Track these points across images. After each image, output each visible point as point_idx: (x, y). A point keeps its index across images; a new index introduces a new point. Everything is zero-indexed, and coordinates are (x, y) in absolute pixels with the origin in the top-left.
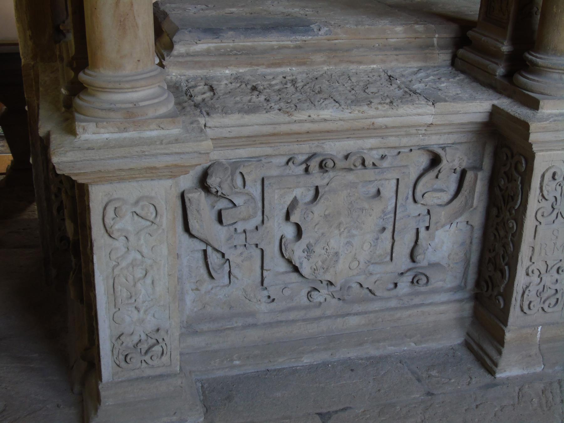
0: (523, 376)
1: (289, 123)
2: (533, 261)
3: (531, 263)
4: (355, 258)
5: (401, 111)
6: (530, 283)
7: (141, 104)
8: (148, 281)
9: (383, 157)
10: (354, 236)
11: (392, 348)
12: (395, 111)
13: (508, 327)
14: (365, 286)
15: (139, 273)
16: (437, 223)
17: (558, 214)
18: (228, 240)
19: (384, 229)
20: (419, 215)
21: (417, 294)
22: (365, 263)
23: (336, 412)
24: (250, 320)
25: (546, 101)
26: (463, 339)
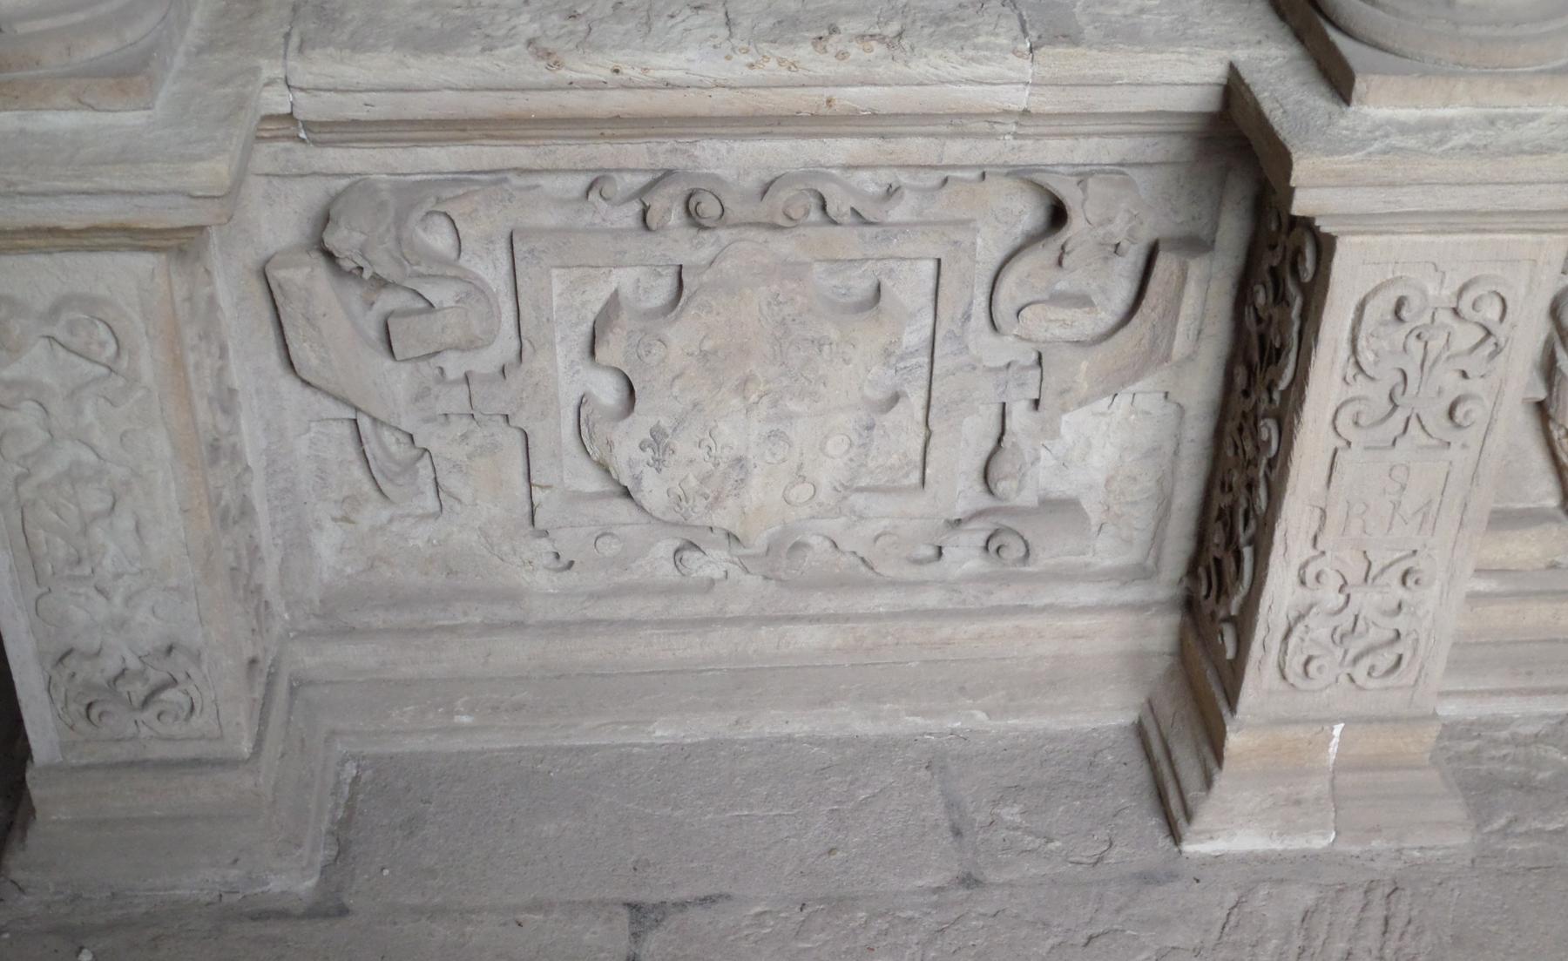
0: (1264, 859)
1: (551, 88)
2: (1320, 546)
3: (1313, 553)
4: (800, 476)
5: (918, 68)
6: (1311, 607)
7: (22, 28)
8: (125, 523)
9: (891, 192)
10: (790, 417)
11: (919, 720)
12: (899, 67)
13: (1238, 716)
14: (845, 545)
15: (95, 501)
16: (1063, 392)
17: (1408, 420)
18: (417, 400)
19: (895, 398)
20: (1009, 365)
21: (1006, 580)
22: (835, 489)
23: (682, 905)
24: (505, 612)
25: (1376, 79)
26: (1127, 718)
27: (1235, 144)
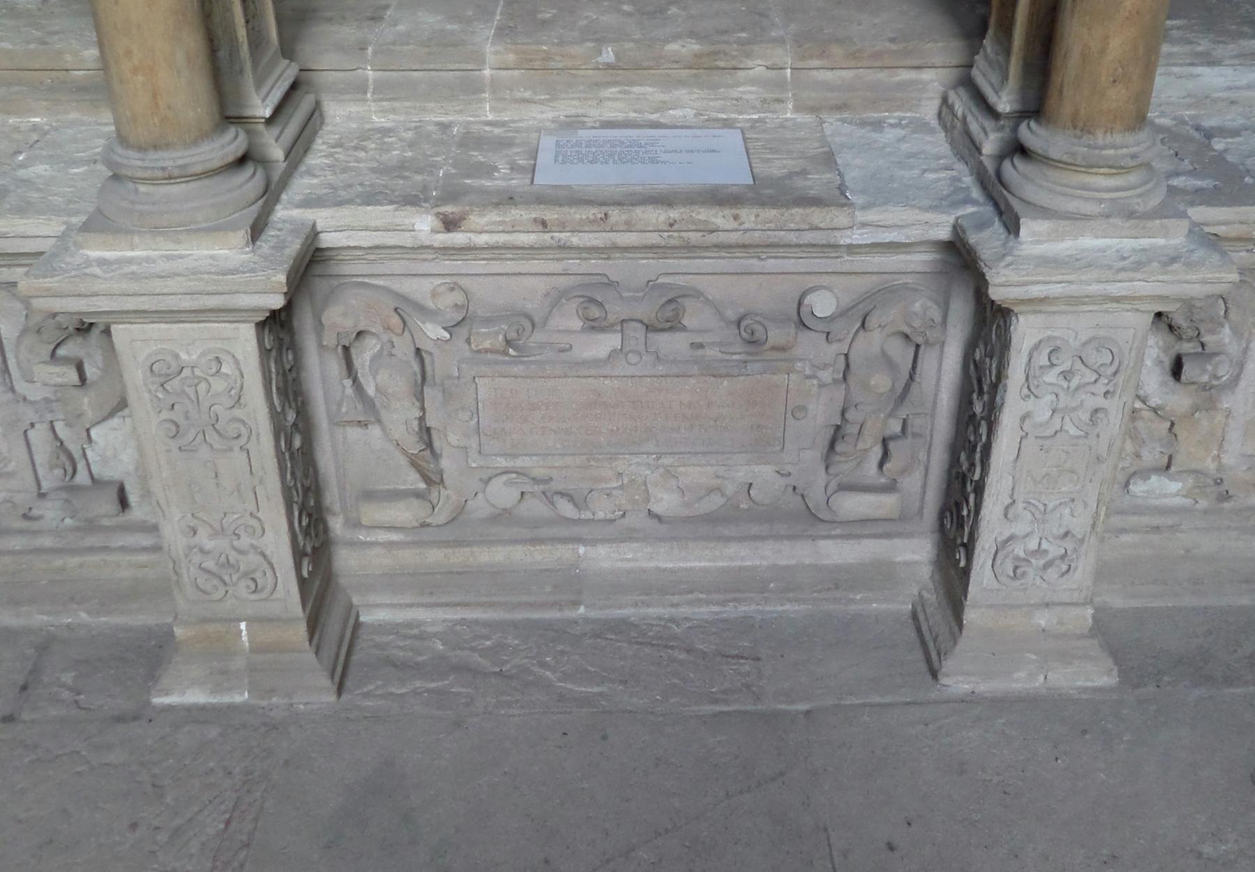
0: (202, 708)
11: (45, 618)
27: (960, 258)
